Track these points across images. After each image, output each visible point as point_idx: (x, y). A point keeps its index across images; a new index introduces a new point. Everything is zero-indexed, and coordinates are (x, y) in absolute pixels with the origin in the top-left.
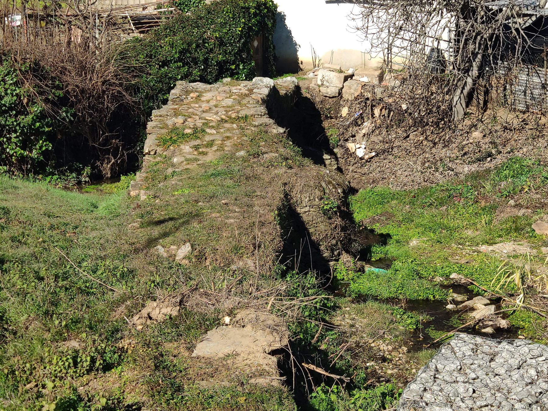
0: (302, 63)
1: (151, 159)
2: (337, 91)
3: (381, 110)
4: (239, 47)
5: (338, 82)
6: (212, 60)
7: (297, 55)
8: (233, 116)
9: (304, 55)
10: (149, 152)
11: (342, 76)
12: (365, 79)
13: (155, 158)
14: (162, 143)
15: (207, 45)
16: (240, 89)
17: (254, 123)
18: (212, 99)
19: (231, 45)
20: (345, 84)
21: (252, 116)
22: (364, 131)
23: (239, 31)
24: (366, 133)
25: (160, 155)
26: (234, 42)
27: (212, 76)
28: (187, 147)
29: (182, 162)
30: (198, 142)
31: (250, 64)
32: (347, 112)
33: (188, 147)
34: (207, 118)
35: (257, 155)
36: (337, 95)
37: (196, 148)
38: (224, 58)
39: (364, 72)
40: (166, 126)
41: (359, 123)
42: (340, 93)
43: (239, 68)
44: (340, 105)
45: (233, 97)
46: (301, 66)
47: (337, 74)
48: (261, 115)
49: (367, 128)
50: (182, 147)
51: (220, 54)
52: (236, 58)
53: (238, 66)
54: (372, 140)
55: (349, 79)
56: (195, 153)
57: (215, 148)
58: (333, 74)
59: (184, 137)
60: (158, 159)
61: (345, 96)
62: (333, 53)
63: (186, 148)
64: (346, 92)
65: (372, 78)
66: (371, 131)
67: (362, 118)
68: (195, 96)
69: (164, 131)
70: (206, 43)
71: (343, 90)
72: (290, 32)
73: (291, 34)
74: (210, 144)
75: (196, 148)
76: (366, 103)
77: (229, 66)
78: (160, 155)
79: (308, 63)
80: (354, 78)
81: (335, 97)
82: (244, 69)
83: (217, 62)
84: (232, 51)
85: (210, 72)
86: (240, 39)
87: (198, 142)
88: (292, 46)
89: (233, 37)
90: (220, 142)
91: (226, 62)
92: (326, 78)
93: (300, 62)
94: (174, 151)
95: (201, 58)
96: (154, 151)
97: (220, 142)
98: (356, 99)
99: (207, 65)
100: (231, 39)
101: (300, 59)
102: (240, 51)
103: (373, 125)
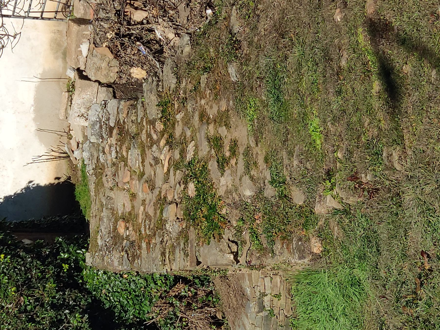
0: (58, 178)
1: (246, 248)
2: (105, 89)
3: (136, 9)
4: (32, 258)
5: (90, 90)
6: (54, 297)
7: (46, 187)
8: (160, 126)
9: (44, 175)
10: (232, 253)
11: (79, 82)
12: (84, 48)
13: (244, 242)
14: (216, 232)
15: (29, 308)
16: (110, 146)
17: (173, 86)
18: (128, 190)
19: (29, 270)
20: (93, 78)
21: (160, 96)
22: (171, 36)
23: (5, 257)
24: (174, 31)
25: (239, 231)
26: (24, 265)
27: (81, 299)
28: (223, 181)
29: (252, 178)
30: (213, 165)
31: (60, 243)
32: (139, 69)
33: (222, 179)
34: (165, 170)
35: (235, 44)
36: (111, 89)
37: (223, 163)
38: (52, 280)
39: (73, 49)
40: (184, 234)
41: (157, 47)
42: (109, 86)
43: (68, 259)
44: (128, 83)
45: (124, 154)
46: (62, 180)
47: (76, 92)
48: (159, 81)
49: (166, 30)
50: (221, 192)
51: (44, 287)
52: (50, 263)
53: (64, 261)
54: (185, 21)
55: (84, 73)
56: (233, 162)
57: (223, 131)
58: (77, 99)
59: (205, 189)
60: (246, 235)
61: (112, 77)
62: (40, 130)
63: (223, 183)
64: (107, 76)
65: (83, 36)
66: (170, 24)
67: (148, 42)
68: (123, 224)
69: (192, 234)
70: (25, 309)
71: (103, 81)
72: (7, 199)
73: (11, 196)
74: (216, 142)
75: (223, 163)
76: (124, 36)
77: (64, 273)
78: (239, 231)
79: (58, 168)
80: (82, 68)
81: (114, 92)
82: (68, 251)
83: (57, 292)
84: (39, 269)
85: (74, 301)
86: (19, 256)
87: (213, 165)
88: (31, 194)
89: (16, 268)
90: (211, 127)
91: (58, 278)
92: (83, 111)
93: (57, 182)
94: (229, 205)
95: (52, 313)
96: (231, 244)
97: (211, 127)
98: (117, 56)
99: (62, 305)
100: (20, 270)
101: (53, 181)
102: (39, 257)
103: (160, 20)
